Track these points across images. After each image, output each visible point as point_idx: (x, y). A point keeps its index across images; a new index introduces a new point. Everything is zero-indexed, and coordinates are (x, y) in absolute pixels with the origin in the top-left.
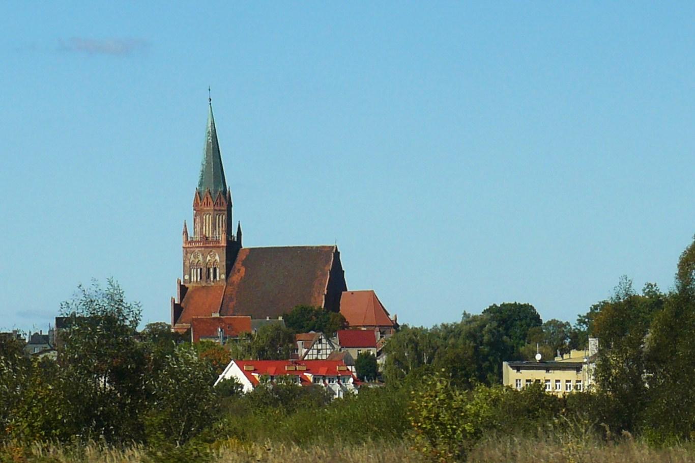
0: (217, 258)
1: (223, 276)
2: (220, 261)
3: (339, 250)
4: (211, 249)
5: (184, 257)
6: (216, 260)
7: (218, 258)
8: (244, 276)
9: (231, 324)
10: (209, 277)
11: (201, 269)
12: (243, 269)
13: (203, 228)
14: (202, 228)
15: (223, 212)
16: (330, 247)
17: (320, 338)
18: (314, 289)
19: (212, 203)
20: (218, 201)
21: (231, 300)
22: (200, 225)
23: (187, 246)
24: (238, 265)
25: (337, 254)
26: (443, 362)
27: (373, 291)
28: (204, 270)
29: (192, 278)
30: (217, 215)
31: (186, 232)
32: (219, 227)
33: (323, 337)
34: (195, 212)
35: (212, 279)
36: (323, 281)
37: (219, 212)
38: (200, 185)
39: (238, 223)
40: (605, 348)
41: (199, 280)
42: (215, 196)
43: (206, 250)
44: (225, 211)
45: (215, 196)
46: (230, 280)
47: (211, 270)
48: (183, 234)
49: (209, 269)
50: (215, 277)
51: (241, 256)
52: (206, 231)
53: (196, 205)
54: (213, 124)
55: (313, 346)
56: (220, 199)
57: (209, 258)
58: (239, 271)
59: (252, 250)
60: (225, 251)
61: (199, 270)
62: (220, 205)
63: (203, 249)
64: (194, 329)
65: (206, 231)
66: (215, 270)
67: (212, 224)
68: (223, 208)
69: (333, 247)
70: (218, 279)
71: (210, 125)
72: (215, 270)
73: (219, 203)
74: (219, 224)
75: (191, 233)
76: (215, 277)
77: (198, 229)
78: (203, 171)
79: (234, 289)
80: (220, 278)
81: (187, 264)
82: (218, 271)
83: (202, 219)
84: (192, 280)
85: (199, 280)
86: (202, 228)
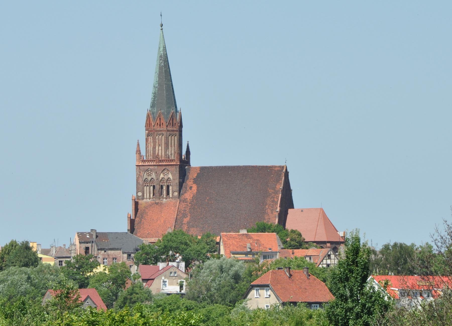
0: (170, 176)
1: (176, 194)
2: (173, 179)
3: (288, 170)
4: (164, 168)
5: (137, 174)
6: (169, 178)
7: (172, 175)
8: (197, 193)
9: (258, 240)
10: (161, 194)
11: (154, 187)
12: (195, 187)
13: (155, 148)
14: (154, 148)
15: (175, 132)
16: (280, 167)
17: (329, 253)
18: (267, 207)
19: (164, 123)
20: (171, 122)
21: (185, 216)
22: (152, 144)
23: (140, 164)
24: (189, 182)
25: (287, 174)
26: (374, 286)
27: (322, 209)
28: (157, 187)
29: (145, 195)
30: (169, 135)
31: (138, 152)
32: (171, 147)
33: (332, 253)
34: (147, 132)
35: (165, 196)
36: (276, 200)
37: (171, 133)
38: (153, 106)
39: (187, 143)
40: (69, 278)
41: (152, 196)
42: (166, 118)
43: (160, 168)
44: (176, 131)
45: (166, 118)
46: (182, 197)
47: (164, 188)
48: (137, 153)
49: (162, 187)
50: (168, 193)
51: (192, 175)
52: (158, 150)
53: (148, 124)
54: (165, 48)
55: (322, 261)
56: (173, 120)
57: (162, 176)
58: (191, 188)
59: (203, 169)
60: (178, 169)
61: (152, 188)
62: (173, 126)
63: (156, 167)
64: (223, 241)
65: (158, 150)
66: (168, 187)
67: (165, 144)
68: (175, 129)
69: (283, 167)
70: (171, 196)
71: (162, 49)
72: (168, 187)
73: (159, 124)
74: (171, 144)
75: (143, 153)
76: (168, 193)
77: (151, 148)
78: (155, 93)
79: (187, 205)
80: (172, 195)
81: (141, 182)
82: (171, 188)
83: (154, 139)
84: (145, 197)
85: (152, 196)
86: (154, 148)
